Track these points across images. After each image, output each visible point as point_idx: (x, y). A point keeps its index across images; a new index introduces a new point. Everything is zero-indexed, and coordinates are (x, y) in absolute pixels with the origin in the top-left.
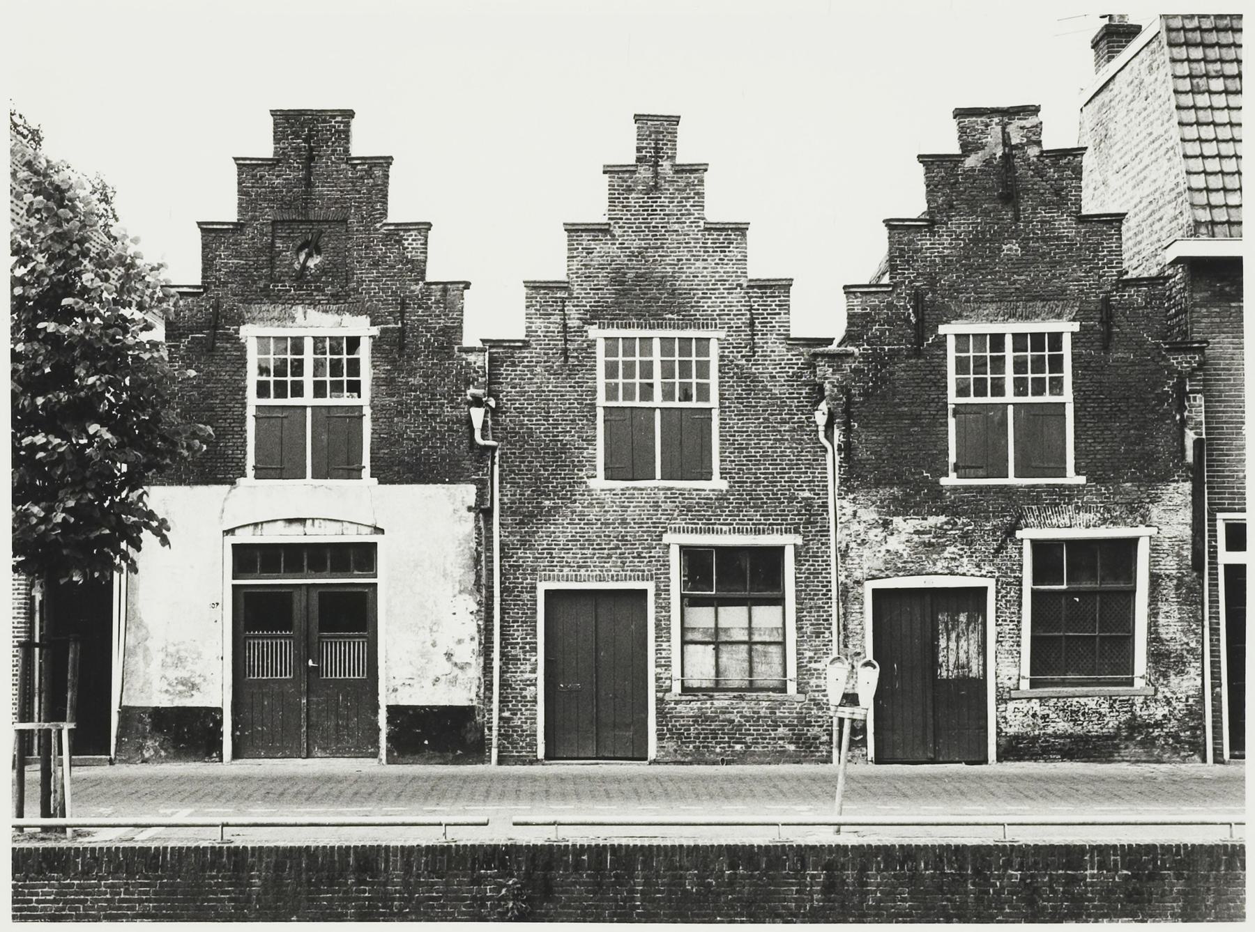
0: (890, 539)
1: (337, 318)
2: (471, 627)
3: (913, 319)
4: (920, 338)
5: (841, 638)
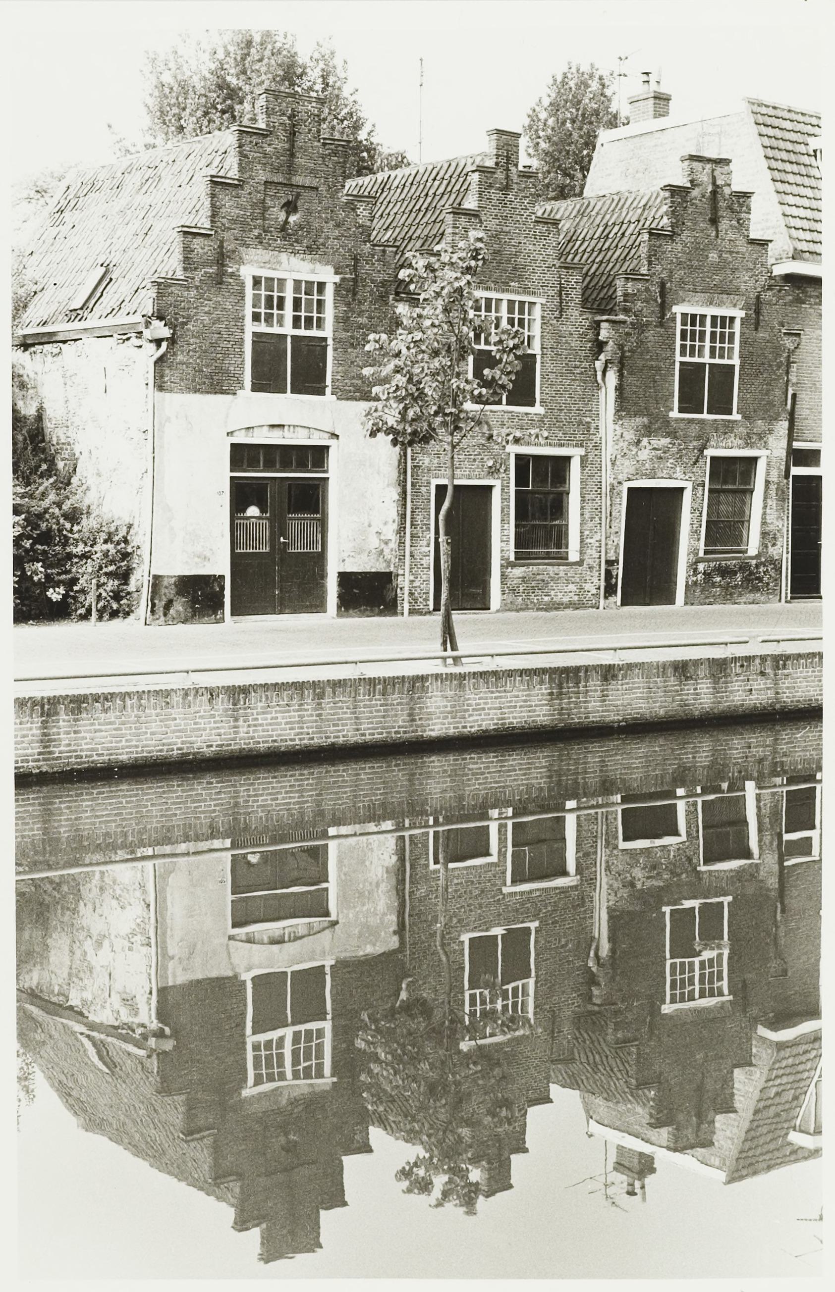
0: (639, 453)
1: (311, 266)
2: (393, 512)
3: (659, 300)
4: (663, 315)
5: (608, 520)
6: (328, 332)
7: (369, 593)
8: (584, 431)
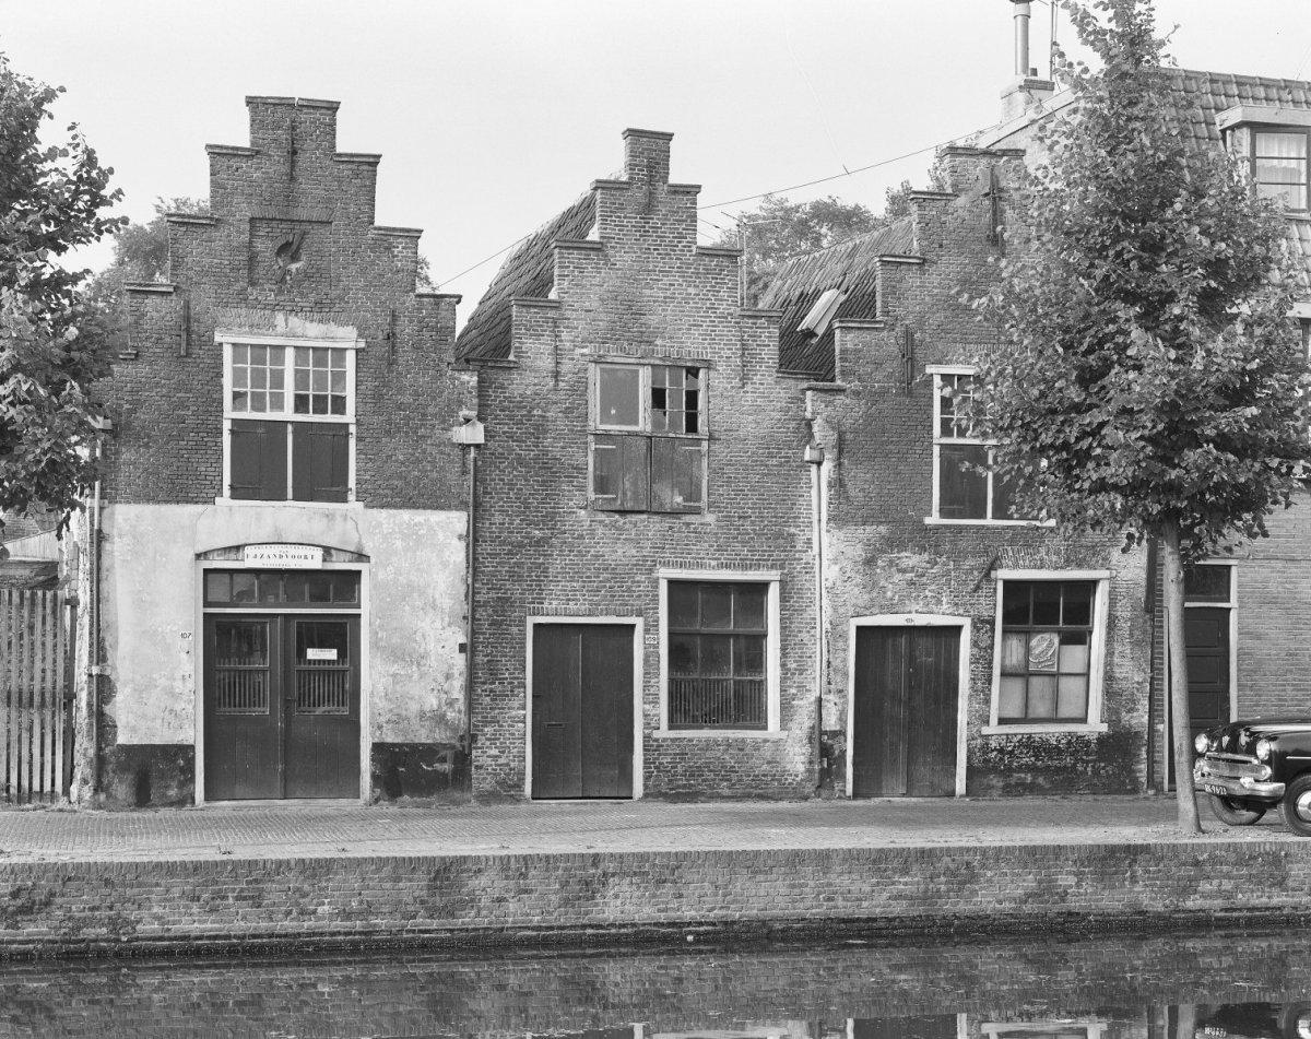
6: (349, 417)
7: (415, 773)
8: (781, 542)
